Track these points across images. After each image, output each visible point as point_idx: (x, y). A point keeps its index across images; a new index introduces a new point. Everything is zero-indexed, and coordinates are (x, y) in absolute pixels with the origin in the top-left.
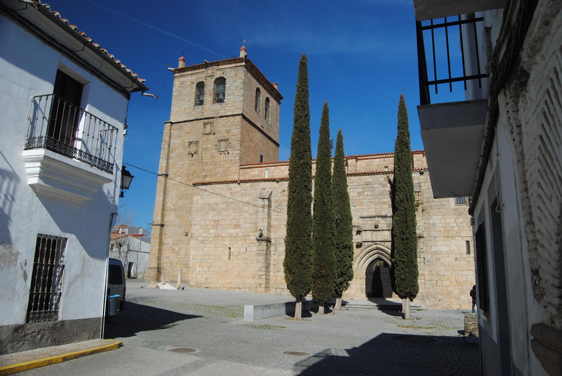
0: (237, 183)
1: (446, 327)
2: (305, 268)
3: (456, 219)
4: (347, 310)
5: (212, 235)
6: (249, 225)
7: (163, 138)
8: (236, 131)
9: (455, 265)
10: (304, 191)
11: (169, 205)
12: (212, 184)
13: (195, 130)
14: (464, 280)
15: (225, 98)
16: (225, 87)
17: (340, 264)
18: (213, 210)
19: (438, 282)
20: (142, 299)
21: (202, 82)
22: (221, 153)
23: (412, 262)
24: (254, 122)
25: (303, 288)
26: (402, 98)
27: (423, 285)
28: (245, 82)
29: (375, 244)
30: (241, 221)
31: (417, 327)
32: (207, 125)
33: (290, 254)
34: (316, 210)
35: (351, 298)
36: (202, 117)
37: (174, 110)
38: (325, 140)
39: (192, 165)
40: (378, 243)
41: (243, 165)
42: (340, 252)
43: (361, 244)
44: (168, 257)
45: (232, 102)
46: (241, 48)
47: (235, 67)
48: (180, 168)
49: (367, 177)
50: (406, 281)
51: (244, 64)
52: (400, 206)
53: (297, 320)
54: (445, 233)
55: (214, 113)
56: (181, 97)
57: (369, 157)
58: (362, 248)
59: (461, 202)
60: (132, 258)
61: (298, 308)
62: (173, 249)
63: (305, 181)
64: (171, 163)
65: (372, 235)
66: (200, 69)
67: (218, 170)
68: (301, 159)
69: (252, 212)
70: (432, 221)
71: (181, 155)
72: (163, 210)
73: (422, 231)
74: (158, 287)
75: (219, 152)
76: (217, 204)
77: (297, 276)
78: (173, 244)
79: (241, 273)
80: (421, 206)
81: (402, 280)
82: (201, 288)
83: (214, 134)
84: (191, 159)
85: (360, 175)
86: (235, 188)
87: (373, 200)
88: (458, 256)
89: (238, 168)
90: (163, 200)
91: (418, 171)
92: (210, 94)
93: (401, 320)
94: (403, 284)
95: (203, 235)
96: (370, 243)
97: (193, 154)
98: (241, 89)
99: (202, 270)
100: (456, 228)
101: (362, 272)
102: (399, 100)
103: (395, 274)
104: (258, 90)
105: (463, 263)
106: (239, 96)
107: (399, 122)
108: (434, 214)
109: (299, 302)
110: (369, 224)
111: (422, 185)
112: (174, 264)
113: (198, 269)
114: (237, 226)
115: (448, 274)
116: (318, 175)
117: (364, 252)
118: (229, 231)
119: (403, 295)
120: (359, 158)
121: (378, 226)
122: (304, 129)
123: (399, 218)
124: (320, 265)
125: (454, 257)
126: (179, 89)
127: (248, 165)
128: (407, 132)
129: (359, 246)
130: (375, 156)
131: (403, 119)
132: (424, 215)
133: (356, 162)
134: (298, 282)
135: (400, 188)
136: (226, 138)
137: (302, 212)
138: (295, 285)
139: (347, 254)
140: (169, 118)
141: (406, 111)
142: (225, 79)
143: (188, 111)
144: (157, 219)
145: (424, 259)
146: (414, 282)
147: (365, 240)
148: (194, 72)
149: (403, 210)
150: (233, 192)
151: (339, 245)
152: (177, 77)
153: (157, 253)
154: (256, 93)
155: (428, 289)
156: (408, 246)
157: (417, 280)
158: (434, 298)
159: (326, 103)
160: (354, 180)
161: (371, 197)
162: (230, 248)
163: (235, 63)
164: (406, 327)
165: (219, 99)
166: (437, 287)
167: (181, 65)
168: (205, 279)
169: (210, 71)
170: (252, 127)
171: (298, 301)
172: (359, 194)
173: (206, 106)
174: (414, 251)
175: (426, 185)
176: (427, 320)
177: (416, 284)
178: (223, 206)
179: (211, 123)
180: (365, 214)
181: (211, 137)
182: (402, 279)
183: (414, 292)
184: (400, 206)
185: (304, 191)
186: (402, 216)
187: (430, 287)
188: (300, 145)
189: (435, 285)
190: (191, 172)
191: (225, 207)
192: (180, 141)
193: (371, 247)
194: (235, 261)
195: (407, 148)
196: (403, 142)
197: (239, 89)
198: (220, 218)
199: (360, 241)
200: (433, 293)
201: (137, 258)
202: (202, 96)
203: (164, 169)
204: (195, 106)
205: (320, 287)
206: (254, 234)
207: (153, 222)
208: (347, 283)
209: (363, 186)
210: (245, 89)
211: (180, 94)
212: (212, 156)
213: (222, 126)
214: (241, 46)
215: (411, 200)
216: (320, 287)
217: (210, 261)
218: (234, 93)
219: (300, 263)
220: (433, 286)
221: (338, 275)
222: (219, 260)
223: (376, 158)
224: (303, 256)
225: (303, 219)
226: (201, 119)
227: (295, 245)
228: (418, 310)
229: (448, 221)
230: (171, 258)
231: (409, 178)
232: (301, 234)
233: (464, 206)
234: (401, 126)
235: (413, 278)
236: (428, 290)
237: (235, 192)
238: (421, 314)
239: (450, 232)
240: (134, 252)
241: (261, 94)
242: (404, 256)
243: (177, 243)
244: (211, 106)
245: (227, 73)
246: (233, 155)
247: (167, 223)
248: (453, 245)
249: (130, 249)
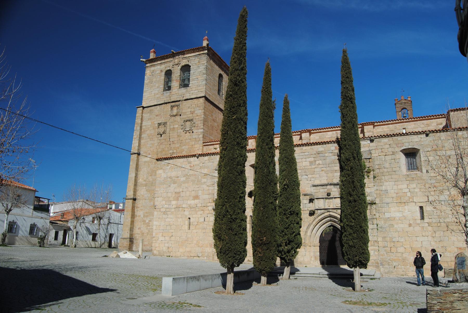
0: (196, 157)
1: (402, 303)
2: (236, 234)
3: (408, 185)
4: (295, 279)
5: (174, 207)
6: (207, 197)
7: (136, 120)
8: (200, 112)
9: (409, 231)
10: (236, 148)
11: (140, 180)
12: (174, 159)
13: (163, 112)
14: (419, 246)
15: (190, 83)
16: (189, 74)
17: (287, 231)
18: (175, 183)
19: (392, 249)
20: (81, 268)
21: (170, 70)
22: (186, 132)
23: (361, 227)
24: (216, 103)
25: (234, 257)
26: (344, 52)
27: (377, 252)
28: (208, 68)
29: (328, 212)
30: (200, 193)
31: (367, 302)
32: (174, 108)
33: (219, 218)
34: (257, 173)
35: (305, 265)
36: (169, 101)
37: (146, 96)
38: (267, 100)
39: (161, 144)
40: (330, 210)
41: (206, 142)
42: (287, 218)
43: (313, 211)
44: (139, 228)
45: (196, 86)
46: (204, 38)
47: (198, 55)
48: (151, 147)
49: (319, 146)
50: (355, 247)
51: (206, 51)
52: (346, 165)
53: (228, 293)
54: (397, 200)
55: (180, 97)
56: (152, 84)
57: (322, 130)
58: (315, 216)
59: (413, 168)
60: (112, 230)
61: (230, 280)
62: (144, 221)
63: (238, 137)
64: (142, 143)
65: (324, 203)
66: (168, 58)
67: (183, 147)
68: (234, 114)
69: (210, 184)
70: (384, 188)
71: (151, 135)
72: (136, 185)
73: (374, 197)
74: (118, 256)
75: (185, 131)
76: (178, 177)
77: (227, 243)
78: (144, 216)
79: (200, 242)
80: (372, 172)
81: (351, 246)
82: (163, 256)
83: (180, 115)
84: (160, 138)
85: (311, 145)
86: (194, 161)
87: (324, 169)
88: (411, 222)
89: (201, 145)
90: (135, 177)
91: (368, 138)
92: (177, 80)
93: (350, 293)
94: (352, 251)
95: (166, 206)
96: (323, 211)
98: (204, 74)
99: (164, 239)
100: (409, 194)
101: (316, 240)
102: (341, 55)
103: (343, 240)
104: (220, 76)
105: (417, 229)
106: (202, 81)
107: (343, 77)
108: (386, 180)
109: (230, 274)
110: (322, 192)
111: (373, 152)
112: (145, 235)
113: (161, 238)
114: (196, 197)
115: (402, 240)
116: (260, 137)
117: (317, 220)
118: (189, 202)
119: (353, 263)
120: (312, 131)
121: (330, 194)
122: (239, 82)
123: (345, 178)
124: (260, 232)
125: (408, 223)
126: (150, 77)
127: (210, 142)
128: (351, 86)
129: (312, 213)
130: (328, 129)
131: (346, 73)
132: (376, 181)
133: (310, 135)
134: (228, 250)
135: (345, 145)
136: (191, 118)
137: (234, 171)
138: (224, 254)
139: (295, 221)
140: (141, 103)
141: (349, 65)
142: (190, 66)
143: (157, 96)
144: (130, 194)
145: (377, 226)
146: (364, 249)
147: (317, 208)
148: (163, 61)
149: (349, 169)
150: (192, 166)
151: (287, 211)
152: (148, 67)
153: (129, 224)
154: (219, 78)
155: (382, 255)
156: (356, 208)
157: (367, 247)
158: (389, 265)
159: (268, 63)
160: (306, 150)
161: (322, 166)
162: (189, 218)
163: (198, 51)
164: (353, 304)
165: (185, 84)
166: (391, 254)
167: (152, 56)
168: (167, 248)
169: (177, 60)
170: (215, 108)
171: (229, 272)
172: (311, 163)
173: (174, 91)
174: (363, 214)
175: (376, 152)
176: (380, 292)
177: (367, 251)
178: (183, 179)
179: (177, 106)
180: (317, 182)
181: (178, 118)
182: (350, 246)
183: (364, 260)
184: (346, 165)
185: (236, 148)
186: (349, 176)
187: (384, 254)
188: (234, 99)
189: (390, 252)
190: (159, 150)
191: (185, 180)
192: (151, 123)
193: (323, 214)
194: (195, 231)
195: (352, 103)
196: (347, 97)
197: (202, 74)
198: (181, 190)
199: (313, 209)
200: (387, 260)
201: (118, 230)
202: (170, 82)
203: (137, 148)
204: (164, 91)
205: (261, 255)
206: (211, 205)
207: (127, 196)
208: (294, 251)
209: (315, 156)
210: (207, 74)
211: (151, 82)
212: (178, 135)
214: (204, 37)
215: (358, 159)
216: (261, 255)
217: (171, 231)
218: (198, 78)
219: (229, 229)
220: (387, 253)
221: (286, 243)
222: (180, 230)
223: (329, 131)
224: (234, 221)
225: (234, 178)
226: (169, 103)
227: (224, 208)
228: (372, 279)
229: (400, 187)
230: (142, 229)
231: (355, 135)
232: (232, 195)
233: (416, 172)
234: (345, 80)
235: (362, 244)
236: (382, 257)
237: (194, 165)
238: (374, 283)
239: (402, 198)
240: (115, 224)
241: (224, 79)
242: (352, 220)
243: (147, 215)
244: (178, 90)
245: (192, 61)
246: (197, 134)
247: (139, 197)
248: (407, 211)
249: (111, 221)
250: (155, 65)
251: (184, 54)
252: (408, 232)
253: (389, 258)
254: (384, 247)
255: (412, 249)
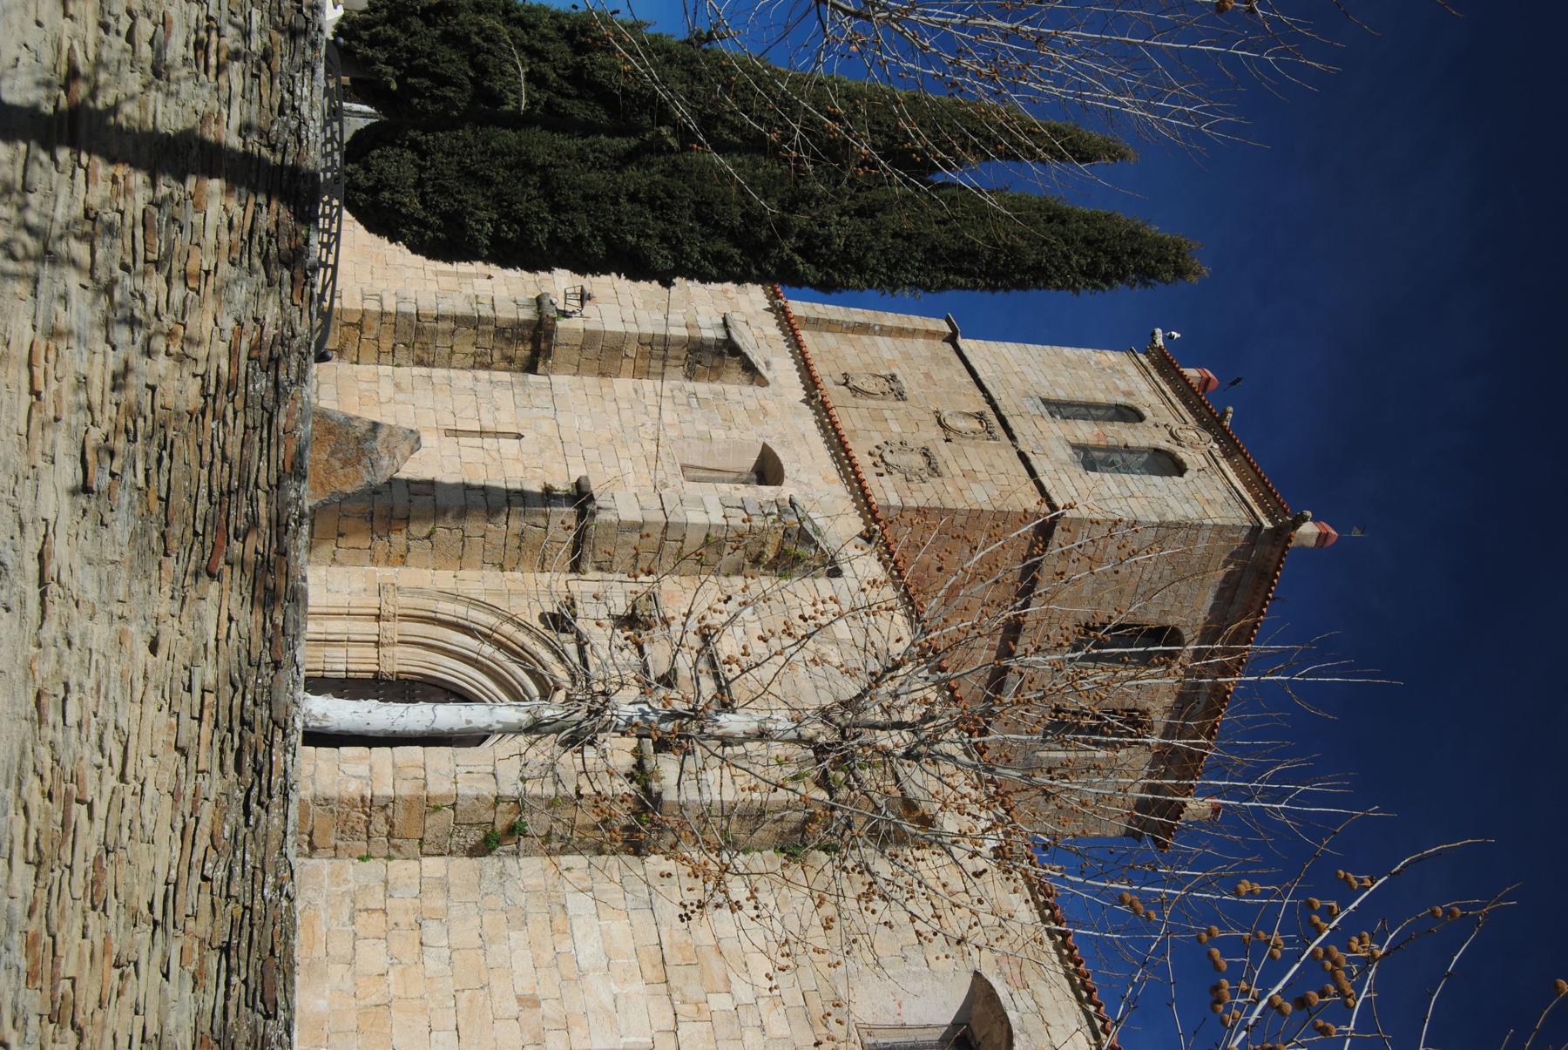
19: (379, 917)
97: (850, 385)
140: (968, 335)
163: (1256, 498)
173: (1053, 427)
187: (346, 881)
189: (359, 906)
213: (987, 461)
239: (694, 971)
250: (1148, 377)
251: (1228, 456)
252: (482, 992)
253: (320, 902)
254: (386, 882)
255: (380, 1009)
